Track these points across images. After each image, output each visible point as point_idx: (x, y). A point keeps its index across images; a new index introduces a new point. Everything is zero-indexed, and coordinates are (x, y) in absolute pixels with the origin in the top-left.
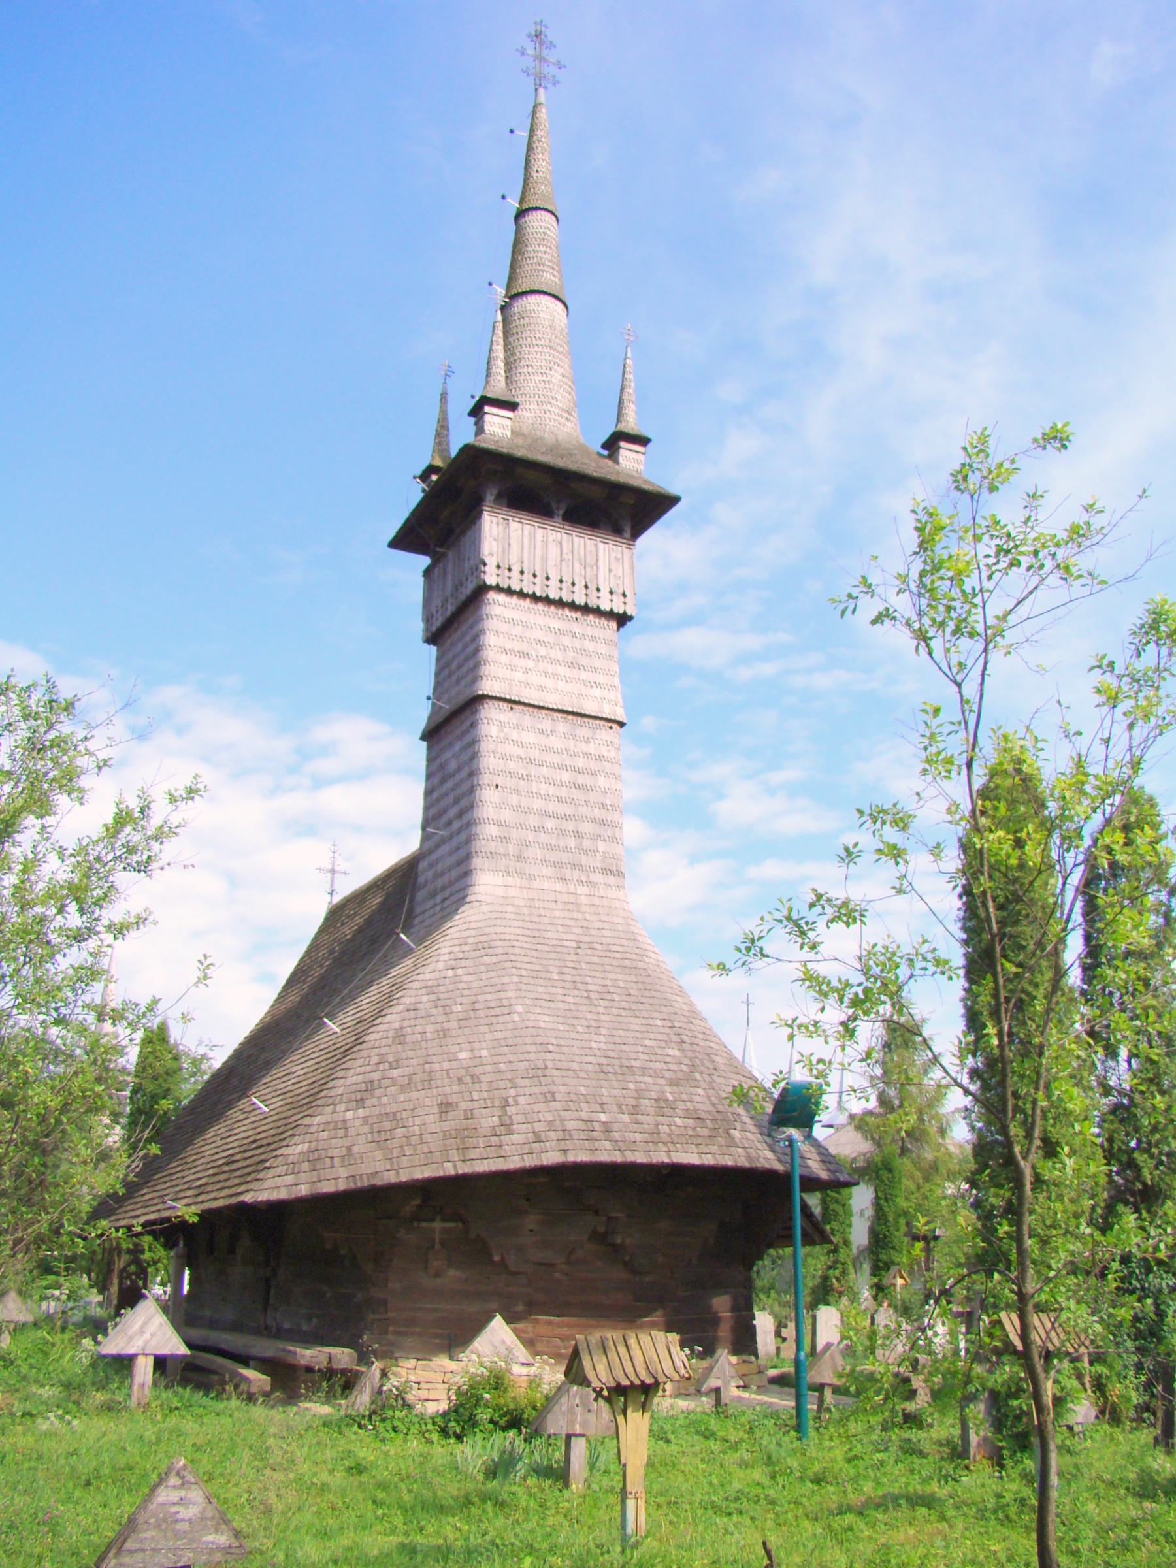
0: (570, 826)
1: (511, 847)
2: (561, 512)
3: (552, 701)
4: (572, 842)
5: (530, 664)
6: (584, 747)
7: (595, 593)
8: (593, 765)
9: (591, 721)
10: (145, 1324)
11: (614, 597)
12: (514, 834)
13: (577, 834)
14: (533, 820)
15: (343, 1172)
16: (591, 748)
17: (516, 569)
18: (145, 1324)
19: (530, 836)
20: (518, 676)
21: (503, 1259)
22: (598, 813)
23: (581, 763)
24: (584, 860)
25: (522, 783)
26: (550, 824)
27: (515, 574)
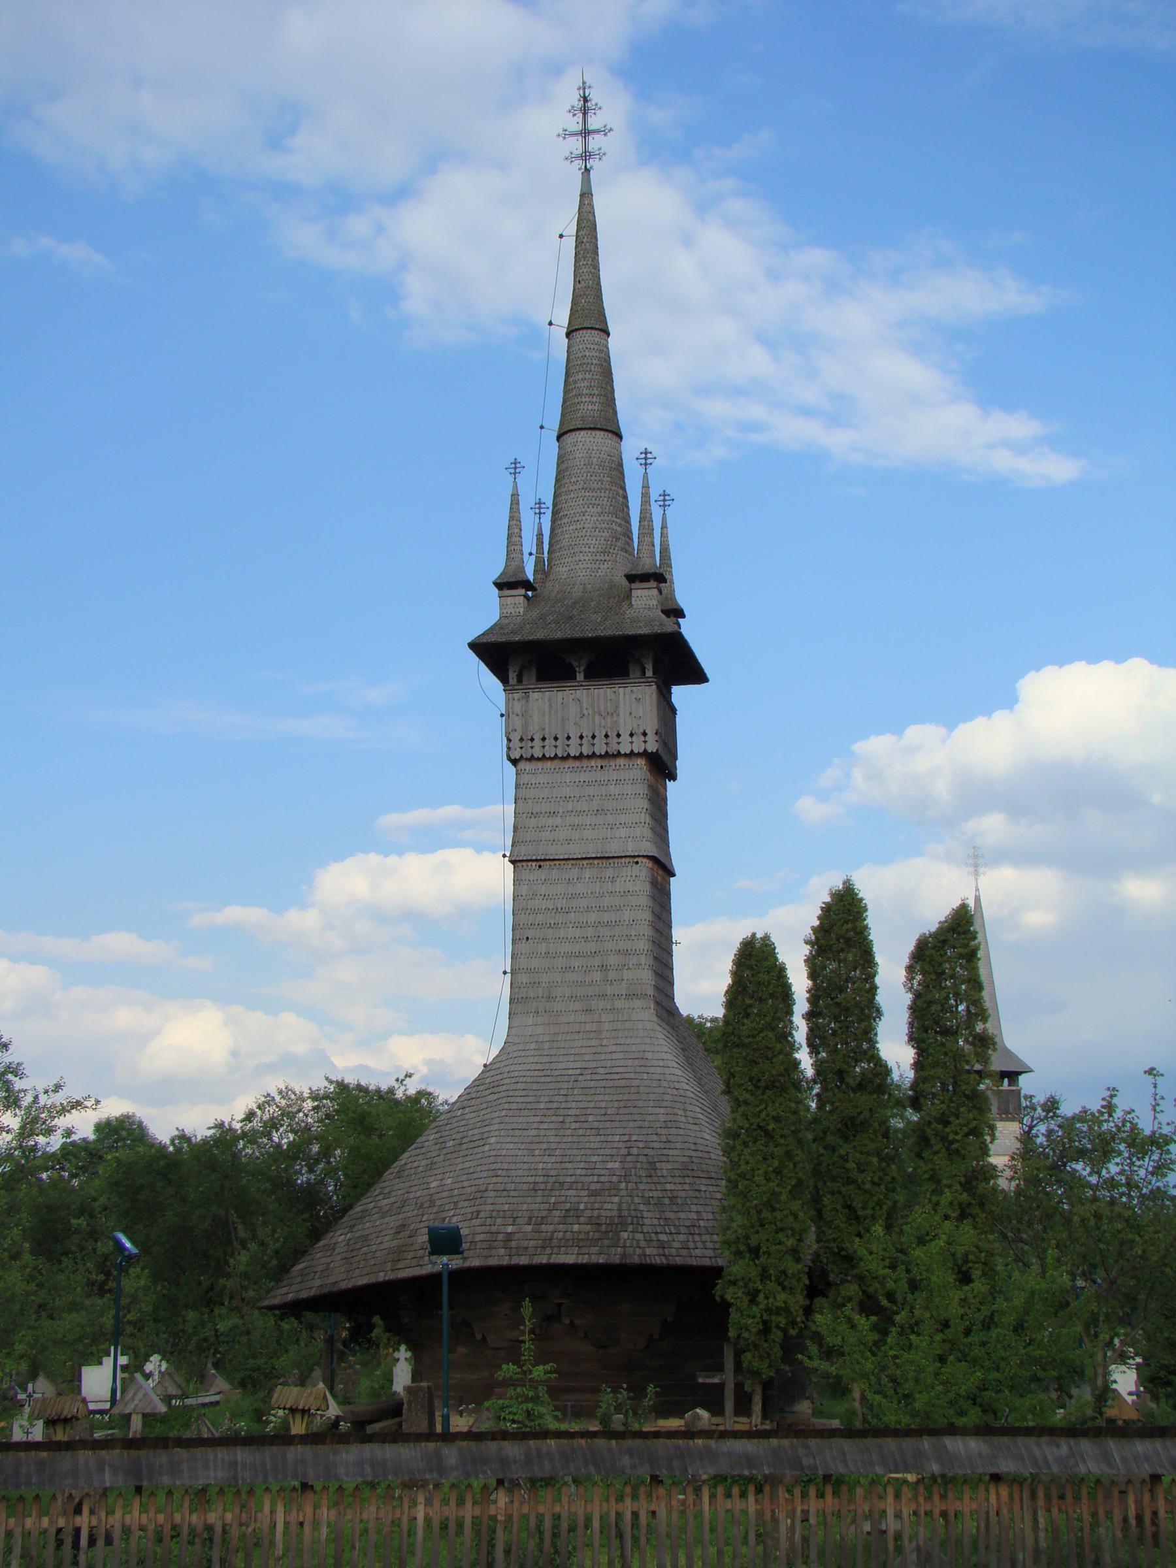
0: (597, 961)
2: (582, 668)
3: (575, 851)
4: (597, 976)
5: (558, 821)
9: (616, 861)
10: (135, 1394)
11: (635, 738)
13: (603, 968)
15: (318, 1283)
16: (618, 886)
17: (537, 737)
18: (135, 1394)
21: (484, 1337)
22: (622, 945)
23: (606, 901)
26: (577, 963)
27: (537, 743)
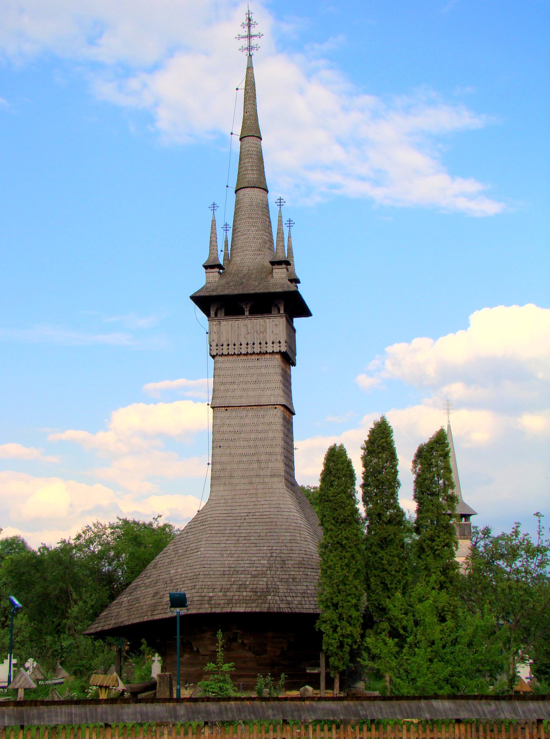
0: (255, 458)
1: (227, 473)
3: (245, 402)
4: (256, 465)
5: (236, 386)
6: (262, 420)
7: (265, 345)
8: (266, 427)
10: (20, 678)
11: (274, 345)
12: (228, 467)
14: (237, 459)
16: (266, 420)
17: (225, 344)
18: (20, 678)
19: (235, 466)
20: (230, 394)
22: (268, 450)
24: (262, 473)
25: (232, 443)
26: (245, 459)
27: (225, 347)
